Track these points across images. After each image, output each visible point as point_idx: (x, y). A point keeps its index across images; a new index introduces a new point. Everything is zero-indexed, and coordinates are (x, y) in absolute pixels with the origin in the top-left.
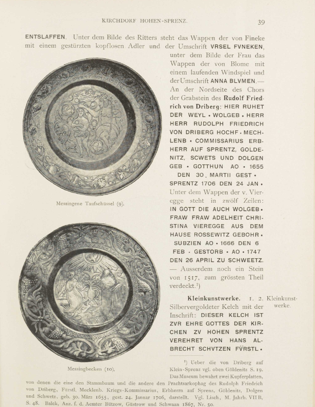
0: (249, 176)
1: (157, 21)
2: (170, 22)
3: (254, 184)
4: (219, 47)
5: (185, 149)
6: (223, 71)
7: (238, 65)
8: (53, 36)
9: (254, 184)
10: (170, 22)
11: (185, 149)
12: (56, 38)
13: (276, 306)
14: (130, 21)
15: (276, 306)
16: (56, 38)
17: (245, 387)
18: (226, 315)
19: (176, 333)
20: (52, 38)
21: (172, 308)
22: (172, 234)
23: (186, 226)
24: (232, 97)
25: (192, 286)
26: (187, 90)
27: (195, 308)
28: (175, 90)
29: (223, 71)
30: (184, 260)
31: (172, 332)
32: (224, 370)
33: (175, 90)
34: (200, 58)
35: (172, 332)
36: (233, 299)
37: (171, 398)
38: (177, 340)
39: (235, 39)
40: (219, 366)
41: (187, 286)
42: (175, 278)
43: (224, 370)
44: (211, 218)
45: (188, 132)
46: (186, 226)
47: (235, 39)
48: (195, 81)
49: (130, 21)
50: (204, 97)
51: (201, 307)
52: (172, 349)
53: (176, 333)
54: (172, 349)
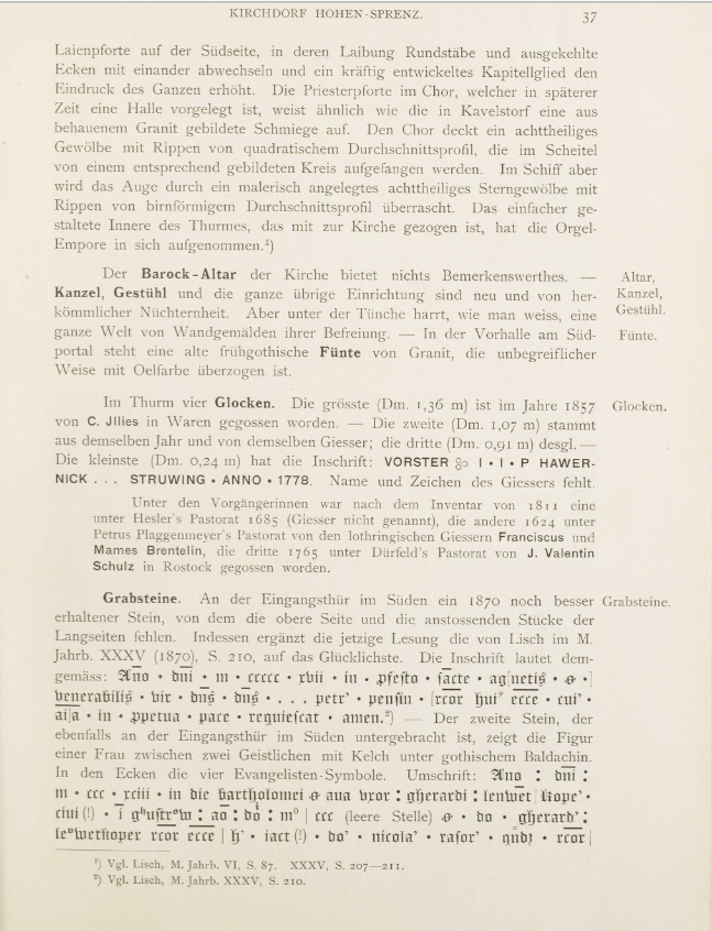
1: (402, 14)
2: (384, 16)
3: (231, 481)
5: (292, 315)
6: (172, 419)
7: (356, 537)
9: (231, 481)
10: (384, 16)
11: (292, 315)
13: (267, 404)
15: (267, 404)
18: (311, 110)
21: (132, 619)
24: (406, 596)
25: (472, 132)
27: (388, 739)
29: (172, 419)
36: (250, 405)
37: (580, 114)
39: (62, 424)
40: (224, 608)
44: (340, 169)
47: (62, 424)
48: (308, 150)
50: (290, 107)
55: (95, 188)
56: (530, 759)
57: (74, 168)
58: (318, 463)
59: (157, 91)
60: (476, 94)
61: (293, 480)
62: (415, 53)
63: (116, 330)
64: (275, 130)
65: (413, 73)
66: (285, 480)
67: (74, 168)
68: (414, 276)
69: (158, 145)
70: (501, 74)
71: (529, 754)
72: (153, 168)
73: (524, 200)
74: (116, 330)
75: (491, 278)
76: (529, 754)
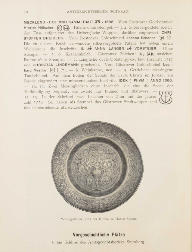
0: (26, 39)
4: (142, 48)
8: (34, 38)
12: (36, 39)
14: (71, 12)
16: (36, 39)
17: (76, 30)
19: (166, 33)
20: (33, 39)
21: (125, 102)
22: (40, 27)
23: (104, 49)
26: (138, 97)
27: (145, 28)
28: (91, 243)
30: (42, 38)
31: (34, 65)
32: (128, 22)
33: (91, 243)
34: (172, 77)
35: (34, 65)
38: (38, 38)
41: (92, 38)
42: (109, 97)
43: (128, 22)
45: (45, 38)
46: (104, 49)
49: (71, 12)
51: (148, 28)
52: (172, 22)
53: (166, 33)
54: (172, 22)
55: (123, 33)
56: (74, 76)
57: (29, 65)
58: (43, 97)
59: (117, 65)
60: (86, 92)
61: (38, 102)
62: (27, 81)
63: (86, 69)
64: (98, 97)
65: (140, 91)
66: (36, 102)
67: (29, 65)
68: (110, 22)
69: (25, 80)
70: (138, 102)
71: (74, 75)
72: (96, 242)
73: (61, 95)
74: (86, 69)
75: (83, 54)
76: (74, 75)
